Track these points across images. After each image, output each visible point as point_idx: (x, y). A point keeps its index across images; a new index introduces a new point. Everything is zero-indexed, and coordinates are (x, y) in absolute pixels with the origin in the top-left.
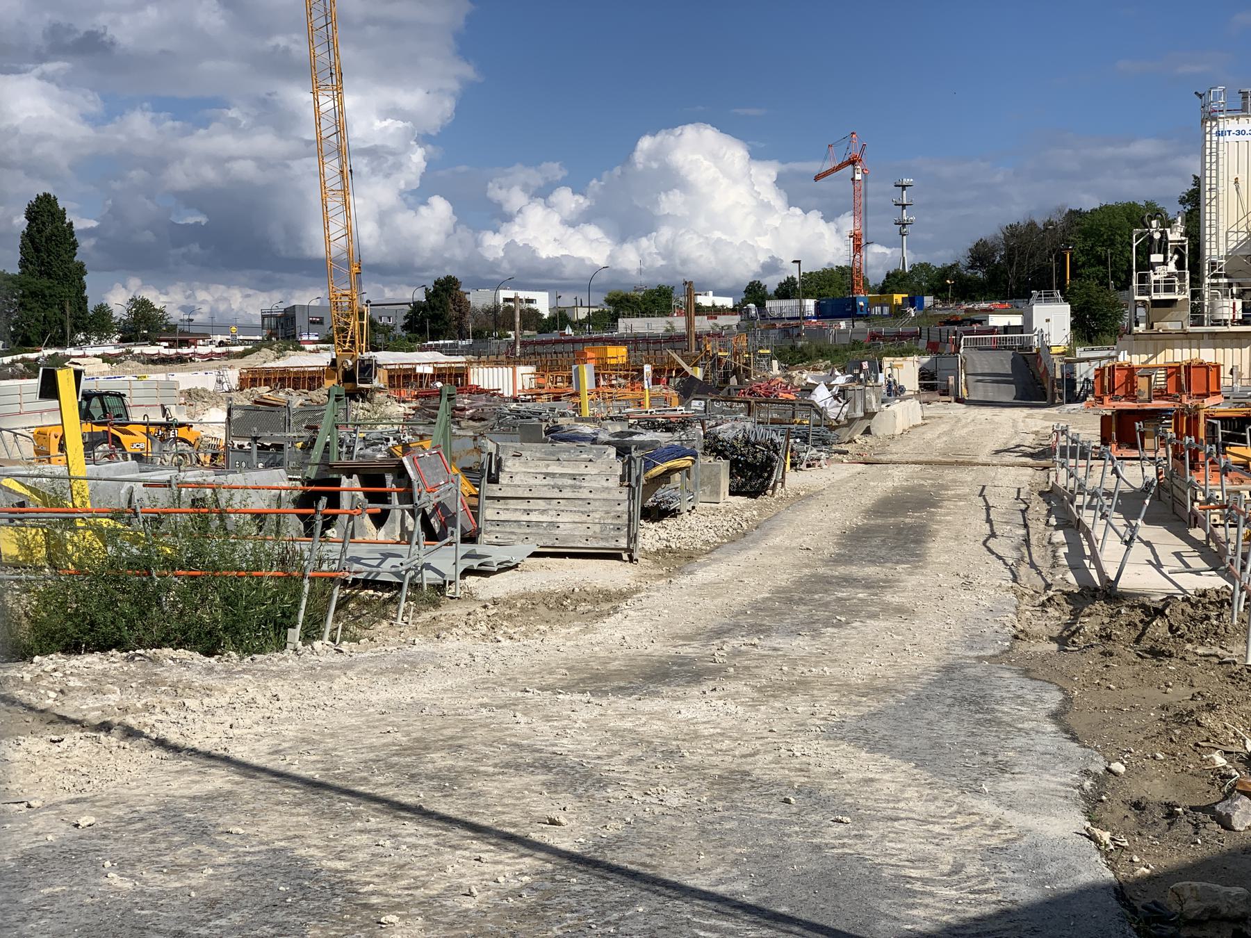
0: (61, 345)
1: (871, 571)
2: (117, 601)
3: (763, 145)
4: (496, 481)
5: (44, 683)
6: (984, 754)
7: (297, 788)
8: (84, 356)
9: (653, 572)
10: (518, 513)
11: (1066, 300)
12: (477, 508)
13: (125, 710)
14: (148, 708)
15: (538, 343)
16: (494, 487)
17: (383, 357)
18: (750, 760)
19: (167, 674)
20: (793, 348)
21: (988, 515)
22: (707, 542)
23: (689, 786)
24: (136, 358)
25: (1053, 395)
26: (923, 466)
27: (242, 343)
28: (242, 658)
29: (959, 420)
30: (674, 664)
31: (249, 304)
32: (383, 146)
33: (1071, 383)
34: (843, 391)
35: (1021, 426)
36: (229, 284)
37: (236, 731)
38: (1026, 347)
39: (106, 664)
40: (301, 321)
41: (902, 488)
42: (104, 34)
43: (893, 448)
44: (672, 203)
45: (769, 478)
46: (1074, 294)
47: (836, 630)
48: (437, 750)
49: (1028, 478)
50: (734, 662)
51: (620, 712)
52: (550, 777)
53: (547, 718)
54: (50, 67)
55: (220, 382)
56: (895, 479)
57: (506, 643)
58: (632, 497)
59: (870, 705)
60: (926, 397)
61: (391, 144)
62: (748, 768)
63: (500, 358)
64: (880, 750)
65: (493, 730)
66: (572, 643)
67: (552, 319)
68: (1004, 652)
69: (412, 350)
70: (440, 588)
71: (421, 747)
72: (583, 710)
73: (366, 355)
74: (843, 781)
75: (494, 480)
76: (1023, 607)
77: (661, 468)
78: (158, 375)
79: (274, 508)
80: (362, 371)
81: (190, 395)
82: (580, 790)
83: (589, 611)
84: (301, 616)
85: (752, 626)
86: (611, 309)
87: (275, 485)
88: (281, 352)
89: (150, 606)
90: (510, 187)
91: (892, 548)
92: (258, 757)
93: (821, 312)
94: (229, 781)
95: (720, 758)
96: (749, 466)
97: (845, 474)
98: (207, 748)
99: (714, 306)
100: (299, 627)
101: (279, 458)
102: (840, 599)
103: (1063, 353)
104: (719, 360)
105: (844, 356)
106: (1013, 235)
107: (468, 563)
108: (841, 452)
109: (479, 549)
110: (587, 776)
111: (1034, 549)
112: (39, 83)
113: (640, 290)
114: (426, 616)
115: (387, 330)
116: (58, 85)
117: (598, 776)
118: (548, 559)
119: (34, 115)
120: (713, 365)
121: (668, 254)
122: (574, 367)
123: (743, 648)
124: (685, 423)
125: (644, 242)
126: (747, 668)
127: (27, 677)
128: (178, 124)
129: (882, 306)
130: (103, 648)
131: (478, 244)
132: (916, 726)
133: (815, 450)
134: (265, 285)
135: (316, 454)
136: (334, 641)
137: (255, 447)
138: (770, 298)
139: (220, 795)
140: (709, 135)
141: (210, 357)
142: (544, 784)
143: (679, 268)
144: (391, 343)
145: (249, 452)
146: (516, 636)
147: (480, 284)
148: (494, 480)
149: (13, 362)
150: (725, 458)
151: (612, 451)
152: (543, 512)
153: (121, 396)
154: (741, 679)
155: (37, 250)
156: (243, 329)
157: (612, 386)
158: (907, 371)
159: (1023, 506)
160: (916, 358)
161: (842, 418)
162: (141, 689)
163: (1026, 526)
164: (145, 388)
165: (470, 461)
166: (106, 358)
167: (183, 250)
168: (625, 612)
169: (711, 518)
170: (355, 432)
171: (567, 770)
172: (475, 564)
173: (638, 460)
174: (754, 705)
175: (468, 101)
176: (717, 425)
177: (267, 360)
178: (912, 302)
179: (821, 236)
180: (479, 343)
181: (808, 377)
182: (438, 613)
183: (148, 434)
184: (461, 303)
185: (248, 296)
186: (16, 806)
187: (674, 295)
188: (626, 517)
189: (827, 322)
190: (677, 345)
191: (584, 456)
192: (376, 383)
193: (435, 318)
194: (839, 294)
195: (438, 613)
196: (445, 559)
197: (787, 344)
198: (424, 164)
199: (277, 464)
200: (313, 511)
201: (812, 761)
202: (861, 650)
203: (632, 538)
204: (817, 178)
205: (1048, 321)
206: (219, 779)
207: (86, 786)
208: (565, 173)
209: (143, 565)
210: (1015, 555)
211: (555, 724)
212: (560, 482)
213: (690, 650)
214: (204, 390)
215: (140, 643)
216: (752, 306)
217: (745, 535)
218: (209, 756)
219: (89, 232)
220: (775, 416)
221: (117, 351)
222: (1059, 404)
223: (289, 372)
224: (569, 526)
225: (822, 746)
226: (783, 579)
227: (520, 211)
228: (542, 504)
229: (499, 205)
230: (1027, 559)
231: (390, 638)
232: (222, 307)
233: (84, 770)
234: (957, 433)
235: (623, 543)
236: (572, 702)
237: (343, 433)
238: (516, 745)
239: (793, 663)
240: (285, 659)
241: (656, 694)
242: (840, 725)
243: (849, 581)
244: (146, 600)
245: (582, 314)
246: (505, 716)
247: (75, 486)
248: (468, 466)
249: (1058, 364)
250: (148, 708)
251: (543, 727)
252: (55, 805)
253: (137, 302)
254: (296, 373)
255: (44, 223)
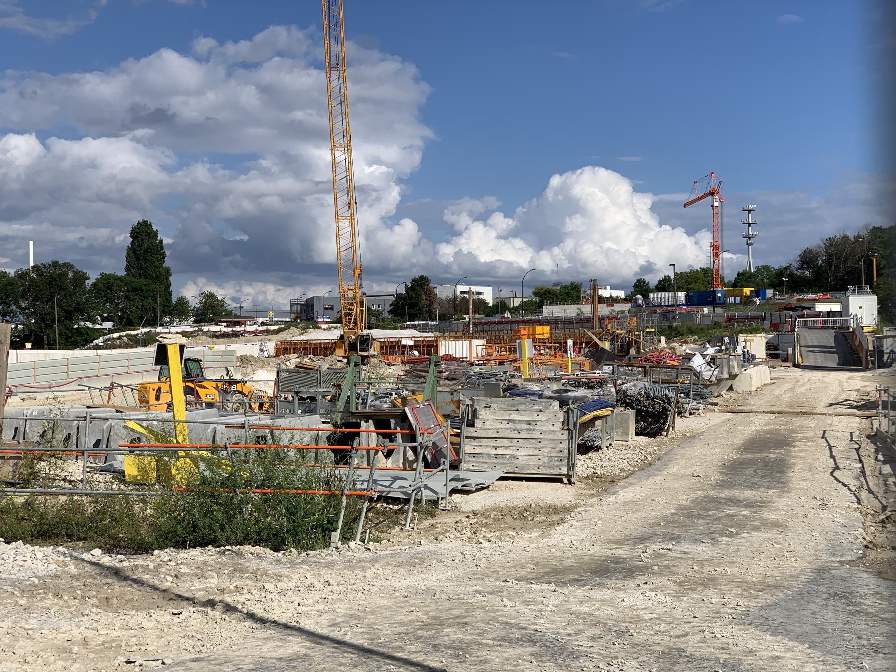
0: (153, 325)
1: (748, 494)
2: (212, 511)
3: (641, 182)
4: (473, 426)
5: (163, 570)
6: (859, 638)
7: (353, 653)
8: (169, 333)
9: (587, 492)
10: (489, 449)
11: (874, 292)
12: (459, 444)
13: (222, 591)
14: (238, 590)
15: (485, 323)
16: (472, 429)
17: (376, 333)
18: (683, 639)
19: (248, 564)
20: (670, 327)
21: (831, 453)
22: (623, 470)
23: (641, 659)
24: (205, 334)
25: (867, 362)
26: (777, 415)
27: (277, 323)
28: (300, 553)
29: (798, 381)
30: (612, 562)
31: (282, 297)
32: (369, 185)
33: (881, 353)
34: (713, 359)
35: (845, 385)
36: (266, 282)
37: (304, 609)
38: (844, 327)
39: (205, 557)
40: (317, 308)
41: (763, 431)
42: (168, 110)
43: (751, 401)
44: (574, 224)
45: (664, 423)
46: (880, 289)
47: (730, 539)
48: (450, 626)
49: (857, 425)
50: (656, 562)
51: (579, 599)
52: (535, 649)
53: (526, 603)
54: (140, 132)
55: (262, 350)
56: (757, 424)
57: (486, 544)
58: (571, 438)
59: (766, 598)
60: (771, 363)
61: (375, 184)
62: (682, 646)
63: (459, 334)
64: (780, 634)
65: (488, 611)
66: (534, 545)
67: (495, 306)
68: (859, 558)
69: (395, 328)
70: (434, 503)
71: (437, 623)
72: (552, 597)
73: (365, 332)
74: (756, 658)
75: (471, 424)
76: (868, 524)
77: (590, 416)
78: (220, 346)
79: (313, 445)
80: (362, 343)
81: (242, 360)
82: (560, 661)
83: (543, 521)
84: (341, 524)
85: (666, 534)
86: (537, 299)
87: (314, 427)
88: (304, 330)
89: (235, 514)
90: (459, 213)
91: (763, 477)
92: (322, 628)
93: (689, 301)
94: (303, 646)
95: (660, 638)
96: (651, 415)
97: (718, 421)
98: (284, 621)
99: (611, 297)
100: (339, 531)
101: (312, 406)
102: (728, 515)
103: (872, 331)
104: (617, 335)
105: (708, 334)
106: (831, 245)
107: (454, 485)
108: (712, 404)
109: (462, 474)
110: (563, 649)
111: (869, 479)
112: (134, 144)
113: (558, 285)
114: (426, 523)
115: (378, 313)
116: (145, 146)
117: (571, 649)
118: (510, 482)
119: (128, 165)
120: (613, 340)
121: (571, 258)
122: (518, 341)
123: (661, 551)
124: (602, 383)
125: (556, 250)
126: (666, 567)
127: (151, 566)
128: (227, 172)
129: (735, 296)
130: (202, 543)
131: (436, 253)
132: (804, 615)
133: (695, 403)
134: (288, 282)
135: (341, 404)
136: (364, 542)
137: (296, 398)
138: (652, 291)
139: (298, 657)
140: (603, 173)
141: (255, 333)
142: (531, 654)
143: (580, 269)
144: (381, 323)
145: (292, 402)
146: (493, 539)
147: (442, 282)
148: (471, 424)
149: (120, 337)
150: (632, 408)
151: (556, 404)
152: (507, 448)
153: (198, 361)
154: (665, 576)
155: (138, 259)
156: (279, 313)
157: (541, 354)
158: (757, 344)
159: (856, 446)
160: (763, 334)
161: (713, 379)
162: (232, 575)
163: (861, 461)
164: (215, 355)
165: (450, 409)
166: (185, 334)
167: (230, 258)
168: (570, 522)
169: (624, 452)
170: (368, 388)
171: (547, 644)
172: (459, 485)
173: (576, 411)
174: (678, 596)
175: (429, 152)
176: (623, 384)
177: (295, 335)
178: (757, 293)
179: (684, 246)
180: (443, 324)
181: (684, 349)
182: (434, 521)
183: (216, 388)
184: (430, 295)
185: (279, 290)
186: (154, 663)
187: (583, 289)
188: (567, 451)
189: (694, 309)
190: (586, 325)
191: (536, 407)
192: (372, 352)
193: (412, 306)
194: (702, 288)
195: (434, 521)
196: (438, 482)
197: (666, 324)
198: (399, 198)
199: (312, 411)
200: (350, 447)
201: (730, 641)
202: (751, 555)
203: (571, 467)
204: (686, 205)
205: (860, 307)
206: (296, 645)
207: (201, 648)
208: (500, 204)
209: (230, 483)
210: (857, 483)
211: (533, 607)
212: (519, 426)
213: (622, 552)
214: (252, 356)
215: (228, 541)
216: (639, 296)
217: (650, 465)
218: (286, 626)
219: (168, 245)
220: (664, 377)
221: (192, 329)
222: (872, 369)
223: (310, 344)
224: (525, 458)
225: (735, 629)
226: (684, 499)
227: (467, 228)
228: (506, 442)
229: (452, 226)
230: (865, 486)
231: (404, 539)
232: (261, 298)
233: (199, 636)
234: (799, 390)
235: (565, 471)
236: (542, 590)
237: (359, 389)
238: (506, 623)
239: (701, 563)
240: (330, 554)
241: (602, 586)
242: (747, 613)
243: (734, 502)
244: (232, 510)
245: (517, 302)
246: (495, 600)
247: (179, 427)
248: (447, 413)
249: (870, 339)
250: (238, 590)
251: (524, 609)
252: (183, 662)
253: (206, 295)
254: (315, 344)
255: (143, 241)
